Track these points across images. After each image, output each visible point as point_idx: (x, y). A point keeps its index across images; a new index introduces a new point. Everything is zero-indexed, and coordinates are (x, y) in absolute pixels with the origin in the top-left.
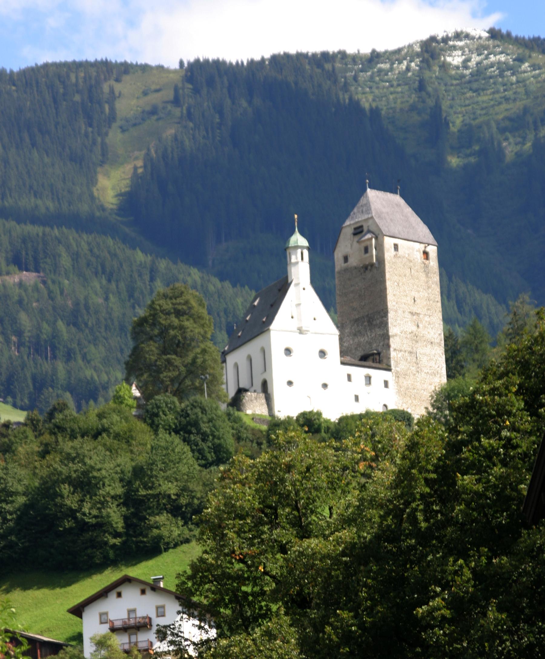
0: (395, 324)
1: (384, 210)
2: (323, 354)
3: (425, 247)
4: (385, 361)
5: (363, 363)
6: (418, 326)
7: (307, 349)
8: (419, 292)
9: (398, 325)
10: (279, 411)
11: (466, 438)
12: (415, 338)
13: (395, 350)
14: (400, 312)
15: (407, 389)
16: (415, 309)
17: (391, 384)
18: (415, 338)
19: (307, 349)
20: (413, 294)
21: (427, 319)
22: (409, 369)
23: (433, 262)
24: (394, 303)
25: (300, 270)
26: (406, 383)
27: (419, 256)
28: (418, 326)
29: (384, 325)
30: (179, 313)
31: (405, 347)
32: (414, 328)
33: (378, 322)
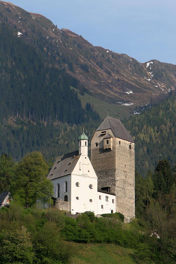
0: (118, 175)
1: (115, 126)
2: (91, 187)
3: (131, 143)
4: (149, 166)
5: (103, 191)
6: (126, 177)
7: (84, 183)
8: (127, 162)
9: (119, 177)
10: (73, 210)
11: (132, 93)
12: (125, 182)
13: (117, 187)
14: (120, 170)
15: (121, 204)
16: (125, 170)
17: (115, 201)
18: (125, 182)
19: (84, 183)
20: (125, 163)
21: (129, 174)
22: (122, 195)
23: (133, 150)
24: (118, 167)
25: (84, 150)
26: (120, 201)
27: (128, 147)
28: (126, 177)
29: (113, 175)
30: (36, 164)
31: (121, 186)
32: (125, 178)
33: (110, 174)
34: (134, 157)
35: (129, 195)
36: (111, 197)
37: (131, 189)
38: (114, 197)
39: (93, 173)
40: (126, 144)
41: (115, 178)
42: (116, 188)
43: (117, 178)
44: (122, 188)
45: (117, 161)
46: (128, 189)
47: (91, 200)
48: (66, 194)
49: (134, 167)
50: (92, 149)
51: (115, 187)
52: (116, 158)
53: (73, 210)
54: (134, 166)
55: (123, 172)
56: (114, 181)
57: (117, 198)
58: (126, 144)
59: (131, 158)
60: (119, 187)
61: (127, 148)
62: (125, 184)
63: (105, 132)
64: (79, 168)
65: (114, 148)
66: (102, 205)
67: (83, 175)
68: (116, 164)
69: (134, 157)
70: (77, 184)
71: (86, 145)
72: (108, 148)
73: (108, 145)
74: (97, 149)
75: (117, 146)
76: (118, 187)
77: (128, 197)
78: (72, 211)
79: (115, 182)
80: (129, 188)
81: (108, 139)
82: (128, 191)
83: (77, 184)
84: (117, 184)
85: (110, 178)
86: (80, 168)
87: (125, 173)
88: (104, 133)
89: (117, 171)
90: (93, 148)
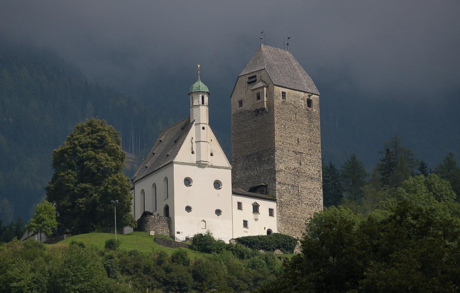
0: (281, 161)
2: (217, 185)
3: (309, 96)
5: (252, 194)
9: (284, 163)
10: (178, 233)
12: (298, 173)
13: (280, 183)
14: (285, 151)
16: (298, 149)
23: (315, 109)
26: (288, 212)
27: (303, 103)
29: (272, 161)
31: (288, 181)
32: (297, 165)
33: (266, 158)
34: (318, 123)
35: (310, 199)
36: (265, 205)
37: (313, 186)
38: (273, 205)
39: (221, 158)
40: (299, 99)
41: (274, 167)
42: (278, 187)
43: (280, 166)
44: (293, 186)
45: (277, 132)
46: (305, 188)
47: (218, 212)
48: (167, 202)
49: (318, 143)
50: (232, 113)
51: (275, 183)
52: (276, 126)
53: (178, 233)
54: (319, 140)
55: (294, 153)
56: (273, 172)
57: (281, 206)
58: (299, 97)
59: (310, 126)
60: (285, 184)
61: (301, 105)
62: (299, 177)
63: (255, 76)
64: (191, 148)
65: (271, 106)
66: (246, 219)
67: (200, 164)
68: (276, 138)
69: (319, 123)
70: (188, 182)
71: (203, 103)
72: (259, 108)
73: (259, 101)
74: (241, 113)
75: (278, 101)
76: (282, 184)
77: (306, 202)
78: (176, 235)
79: (275, 174)
80: (308, 184)
81: (260, 90)
82: (305, 192)
83: (188, 182)
84: (279, 177)
85: (267, 167)
86: (192, 149)
87: (298, 156)
88: (254, 79)
89: (278, 153)
90: (235, 110)
